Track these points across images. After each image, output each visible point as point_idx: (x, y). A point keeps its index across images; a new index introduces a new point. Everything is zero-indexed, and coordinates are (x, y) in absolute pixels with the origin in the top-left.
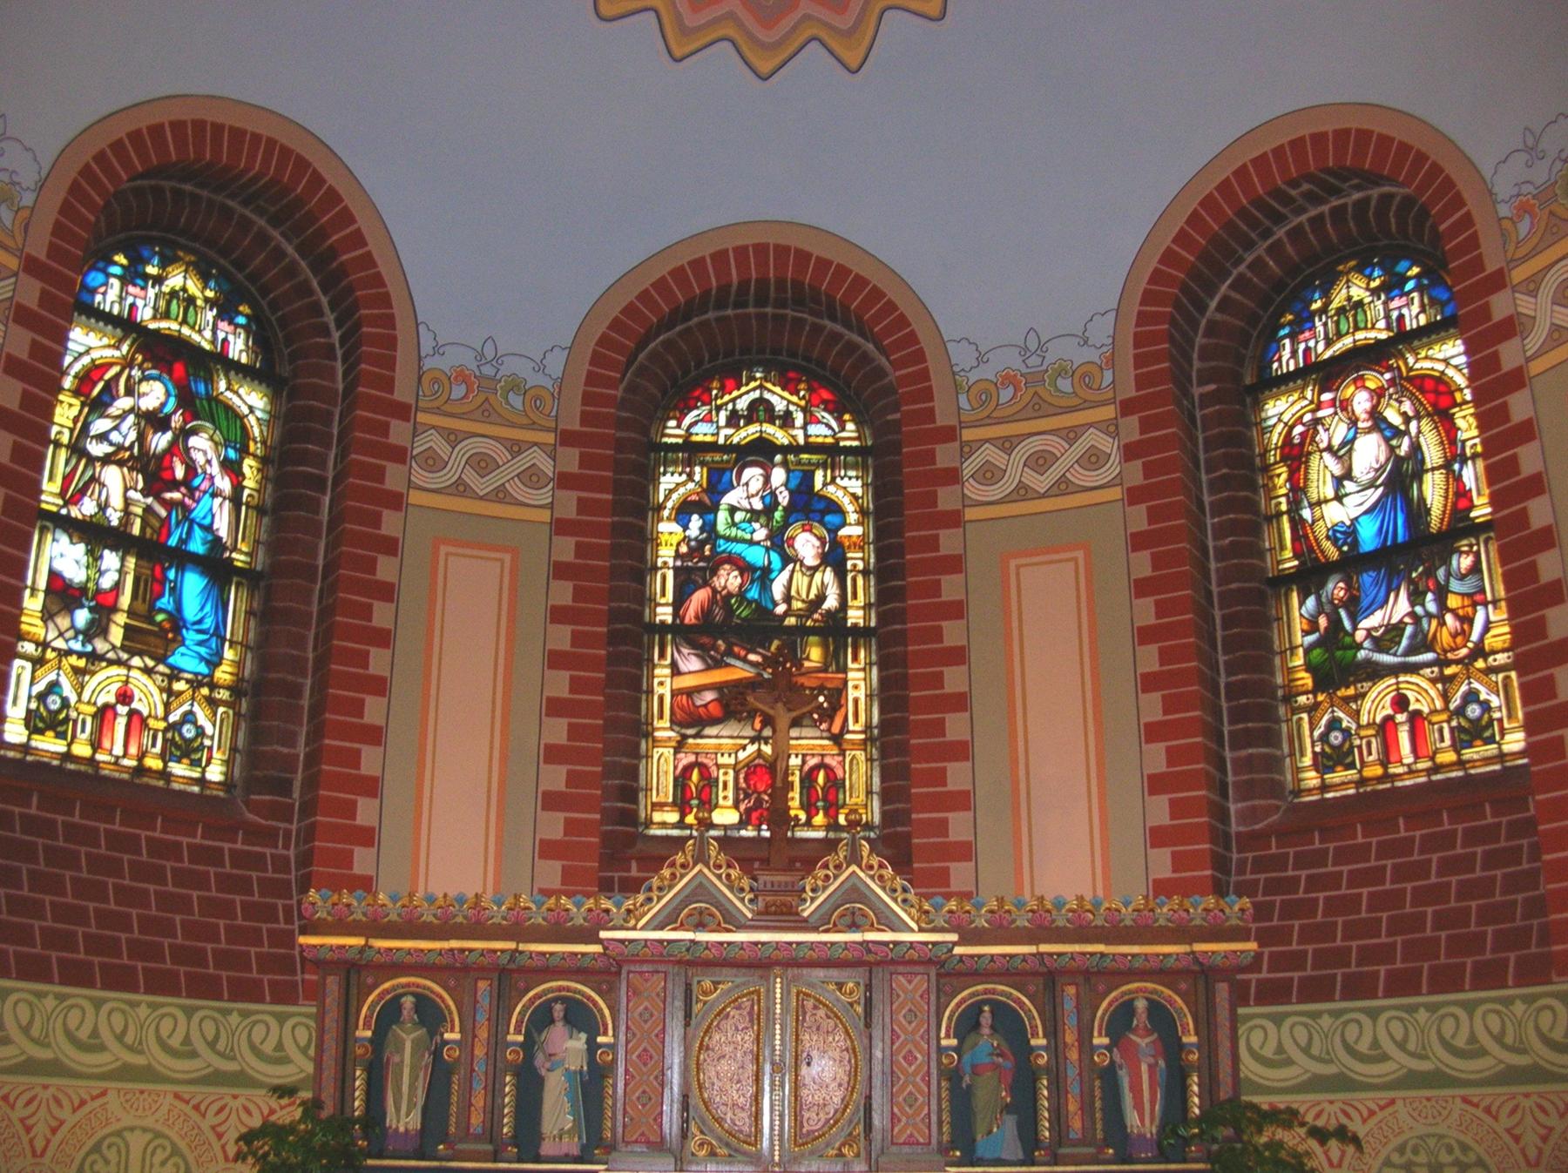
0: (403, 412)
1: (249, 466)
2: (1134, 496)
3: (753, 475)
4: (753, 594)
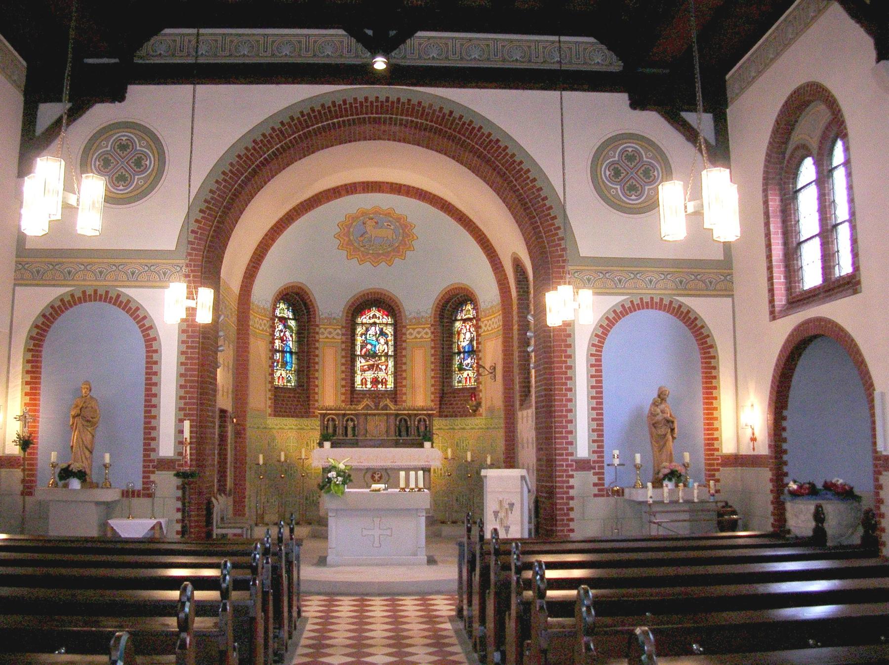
0: (318, 326)
2: (432, 340)
3: (373, 328)
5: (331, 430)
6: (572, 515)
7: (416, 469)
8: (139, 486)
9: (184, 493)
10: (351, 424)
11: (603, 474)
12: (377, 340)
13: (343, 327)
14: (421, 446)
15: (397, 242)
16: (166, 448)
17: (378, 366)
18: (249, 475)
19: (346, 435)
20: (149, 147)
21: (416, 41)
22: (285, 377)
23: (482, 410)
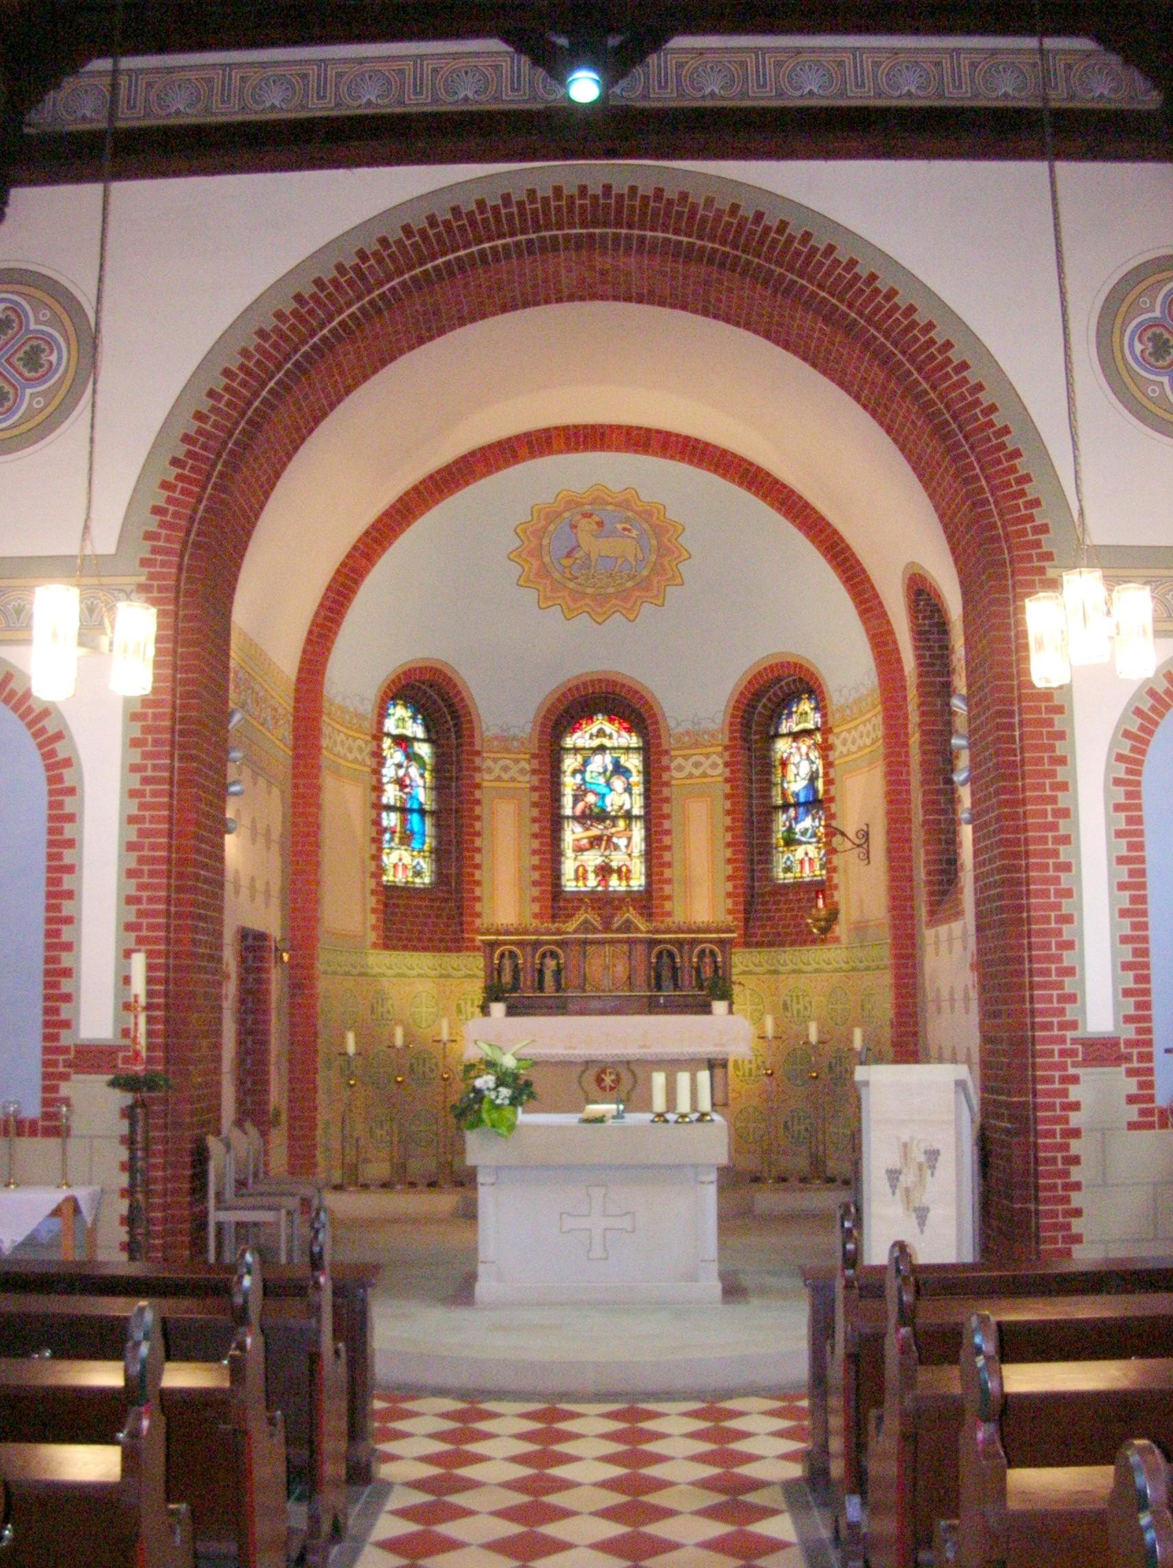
0: (478, 753)
1: (427, 774)
2: (727, 780)
4: (600, 804)
5: (507, 978)
6: (1076, 1174)
7: (692, 1064)
8: (32, 1110)
9: (133, 1125)
10: (551, 964)
11: (1150, 1071)
12: (608, 783)
13: (534, 756)
14: (706, 1009)
15: (643, 567)
16: (96, 1020)
17: (609, 838)
18: (325, 1078)
19: (541, 989)
20: (56, 321)
21: (672, 61)
22: (408, 864)
23: (840, 929)
